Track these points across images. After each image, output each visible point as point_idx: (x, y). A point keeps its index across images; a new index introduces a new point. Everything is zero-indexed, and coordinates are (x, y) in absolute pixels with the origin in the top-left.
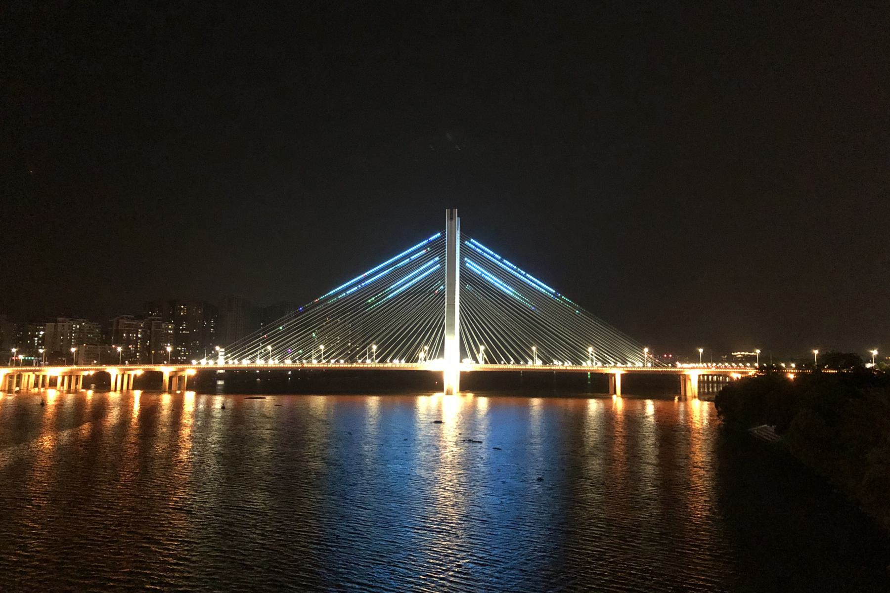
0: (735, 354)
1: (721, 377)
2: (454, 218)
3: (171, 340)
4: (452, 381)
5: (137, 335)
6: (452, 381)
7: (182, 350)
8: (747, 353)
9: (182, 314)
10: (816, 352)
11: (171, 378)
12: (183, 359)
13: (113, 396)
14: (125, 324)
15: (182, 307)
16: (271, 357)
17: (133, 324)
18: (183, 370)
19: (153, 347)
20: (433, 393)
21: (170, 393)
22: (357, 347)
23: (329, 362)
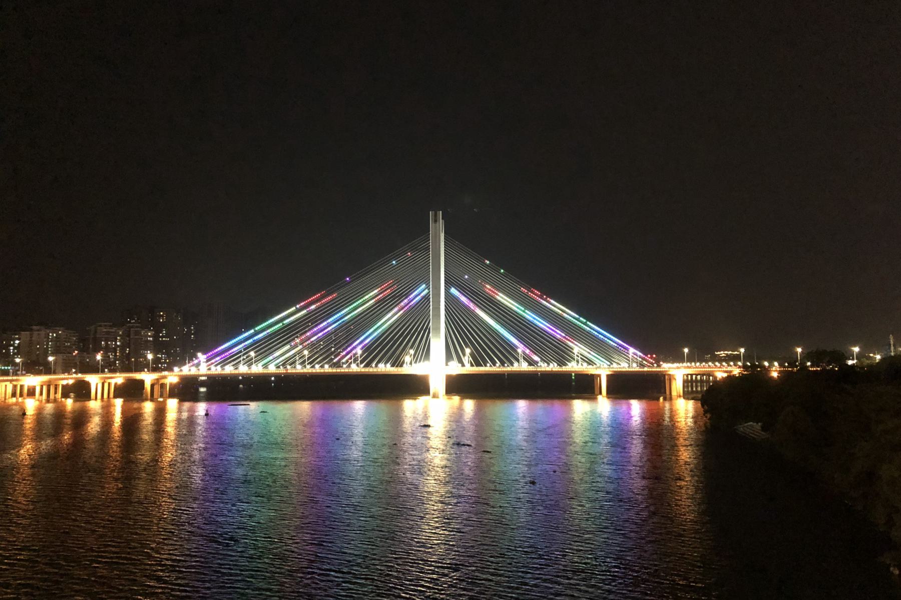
0: (719, 353)
1: (705, 377)
2: (438, 220)
4: (438, 384)
5: (116, 343)
6: (438, 384)
7: (162, 357)
8: (730, 352)
9: (161, 320)
10: (799, 350)
11: (152, 386)
13: (94, 405)
15: (162, 313)
17: (112, 332)
21: (152, 399)
22: (332, 347)
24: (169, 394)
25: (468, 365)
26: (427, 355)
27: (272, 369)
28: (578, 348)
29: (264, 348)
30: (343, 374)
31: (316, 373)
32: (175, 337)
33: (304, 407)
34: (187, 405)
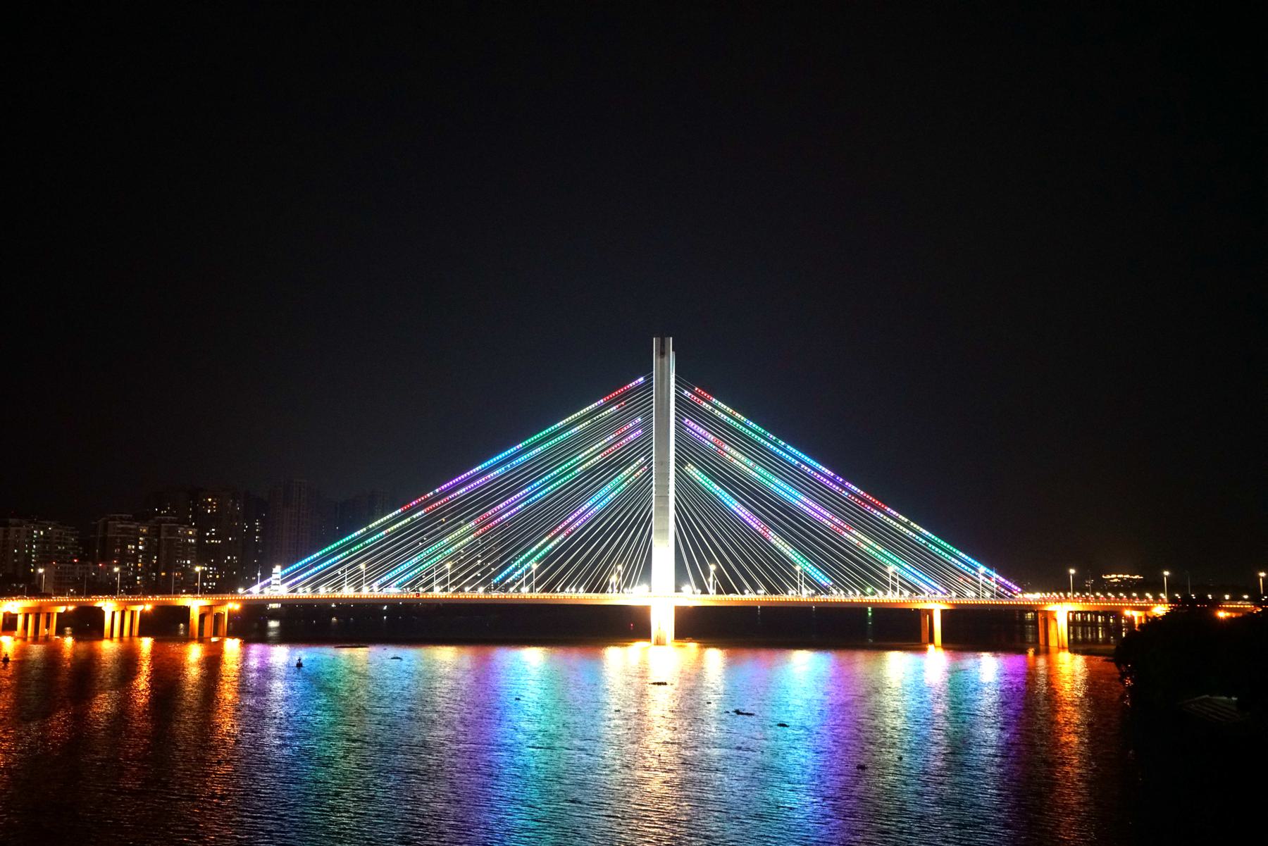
0: (1108, 577)
1: (1089, 616)
2: (666, 351)
3: (193, 554)
4: (663, 623)
5: (137, 546)
6: (663, 623)
7: (209, 570)
8: (1128, 576)
9: (209, 511)
10: (1166, 573)
11: (202, 617)
12: (212, 586)
13: (108, 647)
14: (118, 528)
15: (210, 500)
16: (365, 582)
17: (131, 529)
18: (223, 603)
19: (162, 566)
20: (631, 642)
21: (201, 640)
22: (478, 558)
23: (475, 589)
24: (227, 631)
25: (712, 590)
26: (646, 572)
27: (393, 592)
28: (893, 567)
29: (383, 559)
30: (488, 602)
31: (465, 599)
32: (230, 539)
33: (446, 657)
34: (256, 649)
